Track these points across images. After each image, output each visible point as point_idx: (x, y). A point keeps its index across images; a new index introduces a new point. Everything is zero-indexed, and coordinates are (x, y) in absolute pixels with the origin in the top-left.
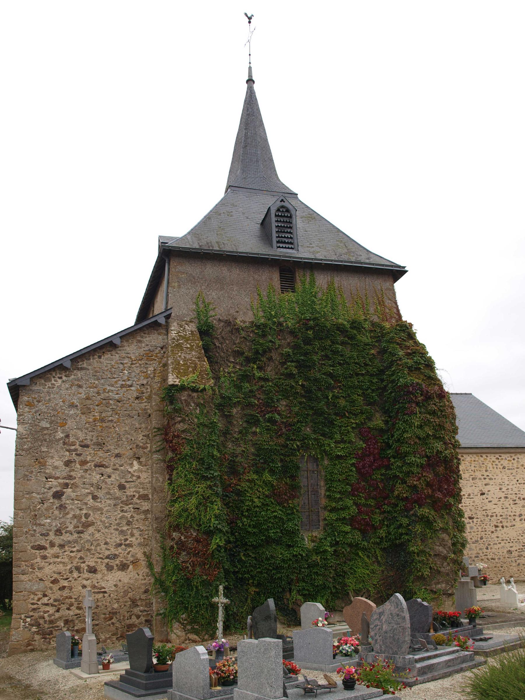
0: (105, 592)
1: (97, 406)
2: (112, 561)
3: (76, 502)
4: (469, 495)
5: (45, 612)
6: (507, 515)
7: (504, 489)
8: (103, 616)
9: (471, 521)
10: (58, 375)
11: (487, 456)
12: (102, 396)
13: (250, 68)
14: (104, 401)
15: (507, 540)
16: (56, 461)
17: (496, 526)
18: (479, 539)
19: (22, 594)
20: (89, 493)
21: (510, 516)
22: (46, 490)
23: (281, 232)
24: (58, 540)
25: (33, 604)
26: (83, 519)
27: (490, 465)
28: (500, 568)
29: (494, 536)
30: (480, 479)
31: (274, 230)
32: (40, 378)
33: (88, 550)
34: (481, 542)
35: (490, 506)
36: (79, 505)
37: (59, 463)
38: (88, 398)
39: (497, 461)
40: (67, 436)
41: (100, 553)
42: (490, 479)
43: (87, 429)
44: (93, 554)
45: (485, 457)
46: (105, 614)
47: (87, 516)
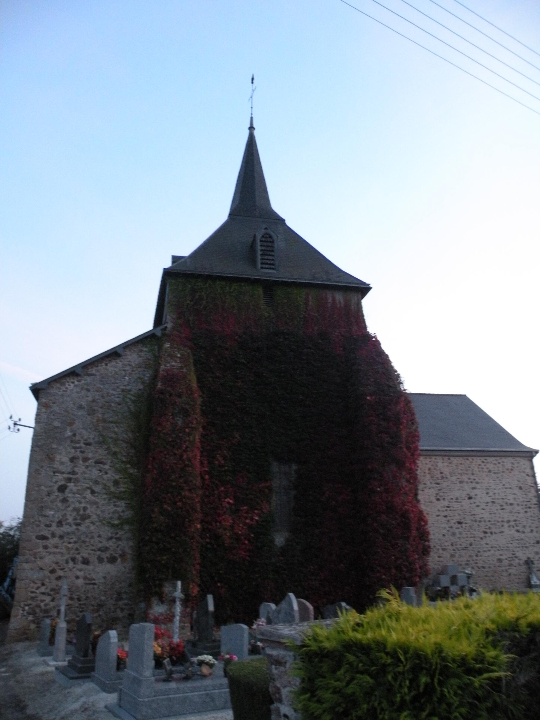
0: (95, 584)
1: (101, 408)
2: (103, 553)
3: (77, 495)
4: (457, 499)
5: (42, 601)
6: (495, 521)
7: (491, 494)
8: (91, 608)
9: (459, 526)
10: (72, 381)
11: (473, 460)
12: (107, 399)
13: (252, 118)
14: (107, 404)
15: (496, 547)
16: (63, 457)
17: (485, 533)
18: (468, 546)
19: (23, 582)
20: (88, 488)
21: (498, 522)
22: (52, 484)
23: (265, 255)
24: (58, 531)
25: (32, 592)
26: (82, 512)
27: (476, 469)
28: (492, 578)
29: (483, 542)
30: (467, 482)
31: (259, 253)
32: (57, 383)
33: (84, 542)
34: (470, 548)
35: (478, 511)
36: (79, 499)
37: (66, 459)
38: (94, 401)
39: (483, 464)
40: (74, 435)
41: (93, 545)
42: (477, 483)
43: (91, 429)
44: (88, 546)
45: (471, 461)
46: (93, 606)
47: (85, 509)
